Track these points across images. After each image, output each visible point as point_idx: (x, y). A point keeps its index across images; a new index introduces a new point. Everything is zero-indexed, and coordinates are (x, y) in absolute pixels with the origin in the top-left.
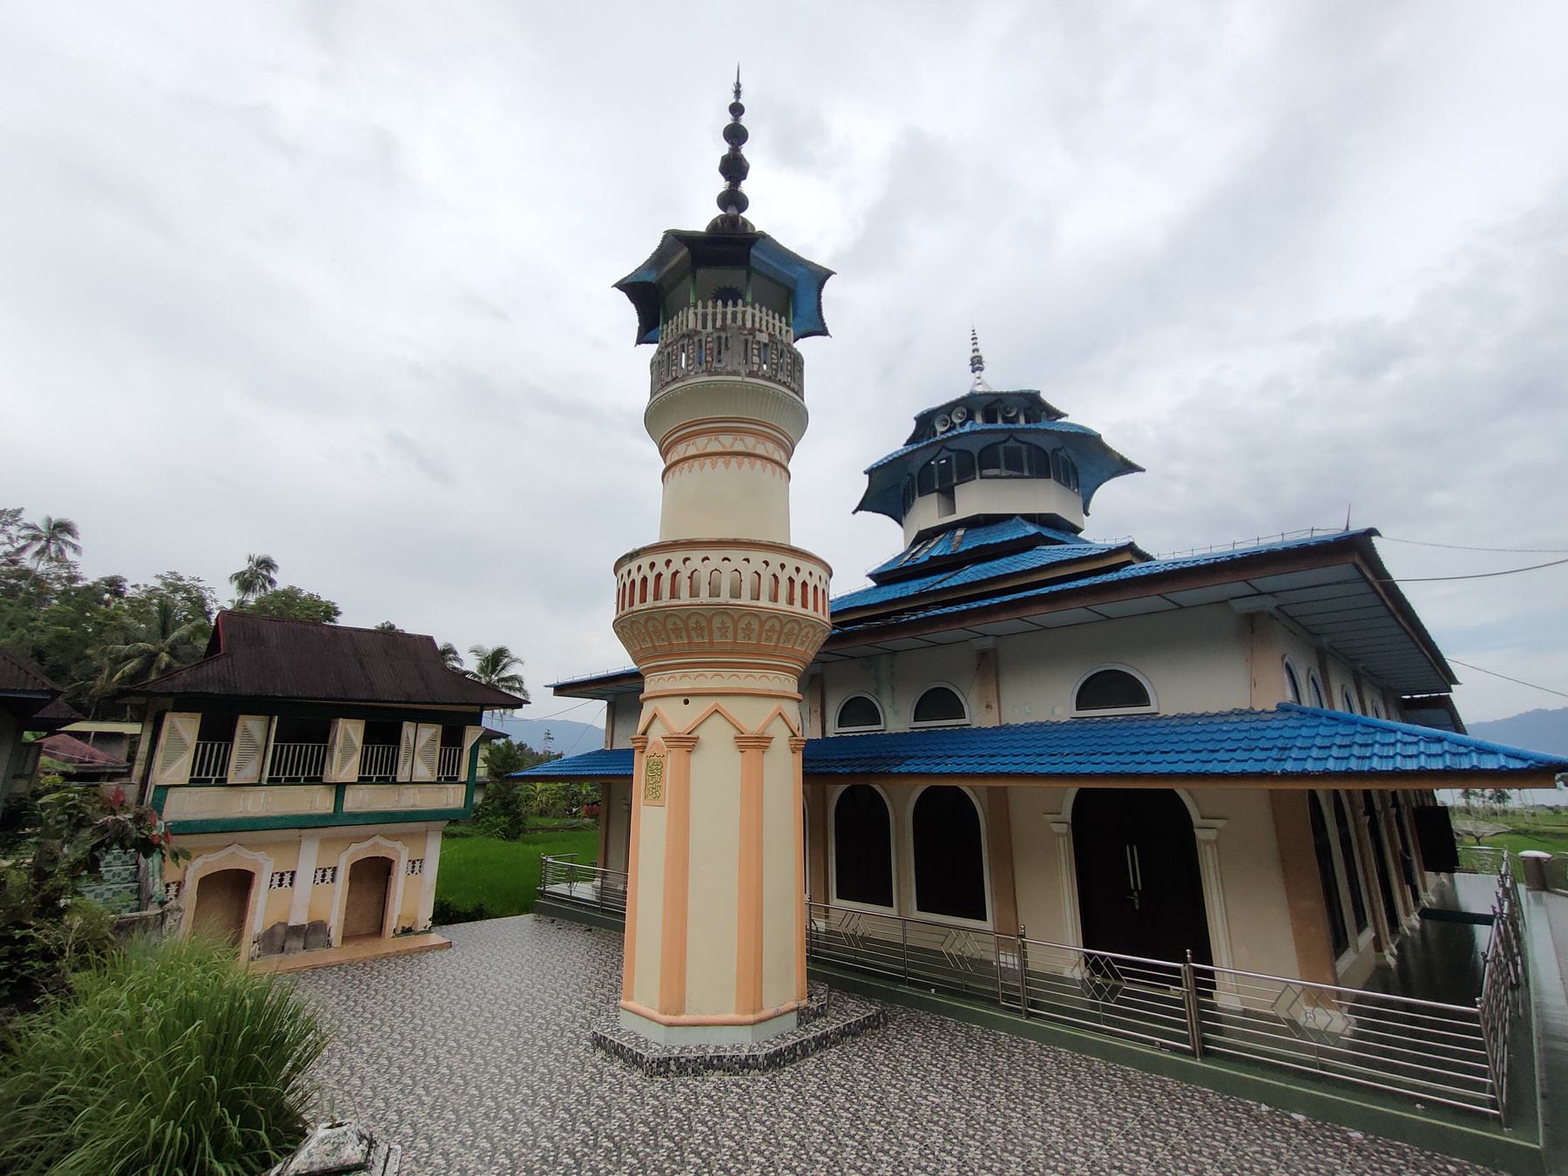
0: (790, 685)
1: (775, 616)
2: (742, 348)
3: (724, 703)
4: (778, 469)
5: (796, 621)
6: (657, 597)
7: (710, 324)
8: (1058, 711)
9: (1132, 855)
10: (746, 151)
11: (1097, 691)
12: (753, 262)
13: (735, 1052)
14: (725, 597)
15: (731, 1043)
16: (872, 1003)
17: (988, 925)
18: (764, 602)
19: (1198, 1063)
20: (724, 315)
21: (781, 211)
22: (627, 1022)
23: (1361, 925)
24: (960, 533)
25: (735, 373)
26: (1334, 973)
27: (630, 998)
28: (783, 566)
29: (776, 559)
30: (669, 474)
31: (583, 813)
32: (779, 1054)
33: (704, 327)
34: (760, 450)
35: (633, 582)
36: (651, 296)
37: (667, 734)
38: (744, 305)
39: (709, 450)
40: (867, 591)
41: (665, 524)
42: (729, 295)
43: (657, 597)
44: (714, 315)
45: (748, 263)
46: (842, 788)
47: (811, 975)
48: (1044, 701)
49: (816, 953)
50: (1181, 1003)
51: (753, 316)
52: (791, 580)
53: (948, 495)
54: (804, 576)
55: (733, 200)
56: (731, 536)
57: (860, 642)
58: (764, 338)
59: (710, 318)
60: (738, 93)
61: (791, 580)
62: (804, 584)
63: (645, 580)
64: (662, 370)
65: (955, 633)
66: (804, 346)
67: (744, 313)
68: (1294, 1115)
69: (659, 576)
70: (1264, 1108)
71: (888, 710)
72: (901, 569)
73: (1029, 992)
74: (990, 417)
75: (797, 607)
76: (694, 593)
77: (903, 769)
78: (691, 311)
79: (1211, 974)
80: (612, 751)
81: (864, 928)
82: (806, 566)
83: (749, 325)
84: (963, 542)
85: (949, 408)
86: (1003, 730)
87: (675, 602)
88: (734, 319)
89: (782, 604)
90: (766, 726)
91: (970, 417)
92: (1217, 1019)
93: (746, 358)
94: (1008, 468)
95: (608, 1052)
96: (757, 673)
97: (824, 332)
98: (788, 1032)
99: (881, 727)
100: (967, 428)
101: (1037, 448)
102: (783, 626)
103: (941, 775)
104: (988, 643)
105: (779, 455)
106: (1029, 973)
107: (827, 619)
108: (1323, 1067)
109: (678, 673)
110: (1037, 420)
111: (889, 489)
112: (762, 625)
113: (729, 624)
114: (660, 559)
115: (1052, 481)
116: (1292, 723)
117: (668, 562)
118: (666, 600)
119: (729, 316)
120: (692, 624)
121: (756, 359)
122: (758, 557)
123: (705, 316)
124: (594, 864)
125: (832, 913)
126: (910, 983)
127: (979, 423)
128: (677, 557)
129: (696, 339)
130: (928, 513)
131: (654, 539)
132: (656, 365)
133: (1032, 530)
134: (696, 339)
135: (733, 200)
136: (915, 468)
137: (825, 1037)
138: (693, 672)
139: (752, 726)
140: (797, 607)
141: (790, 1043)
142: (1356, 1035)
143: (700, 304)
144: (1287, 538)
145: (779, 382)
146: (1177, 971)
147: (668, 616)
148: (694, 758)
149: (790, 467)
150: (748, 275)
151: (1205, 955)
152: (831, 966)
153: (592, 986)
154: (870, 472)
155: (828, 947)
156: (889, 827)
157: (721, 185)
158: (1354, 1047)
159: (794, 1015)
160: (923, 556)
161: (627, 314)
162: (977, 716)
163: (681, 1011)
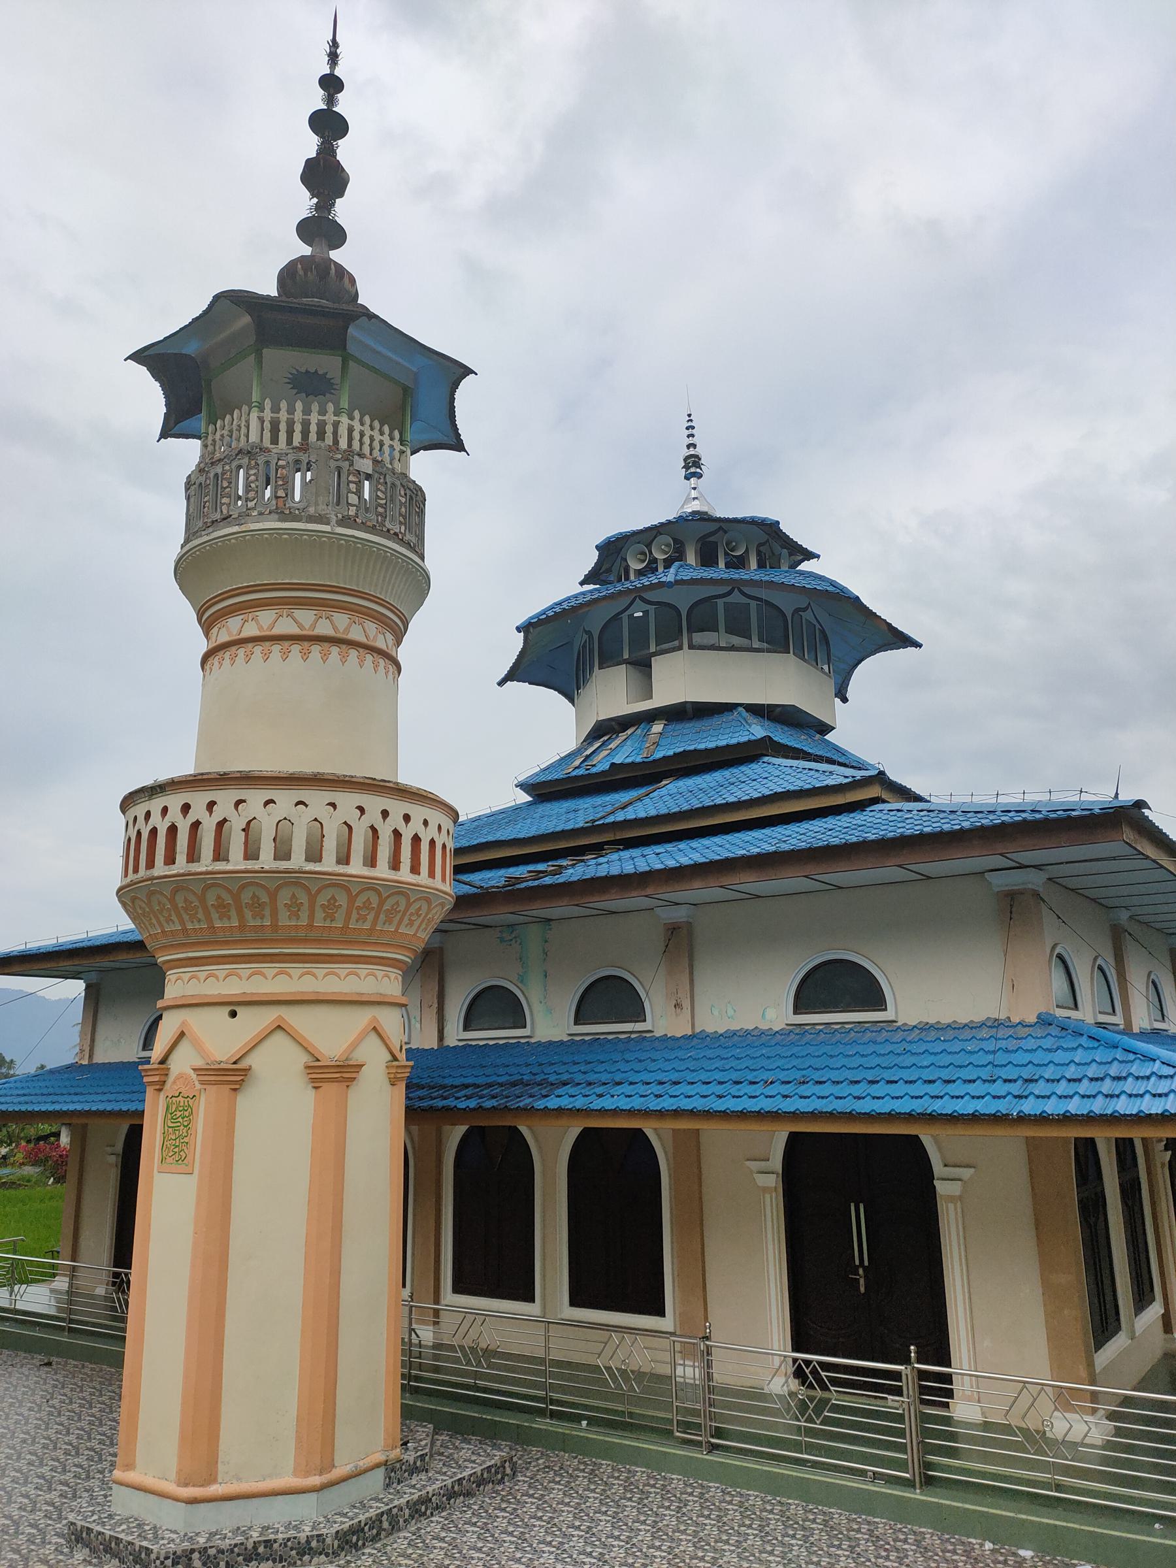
0: (389, 984)
1: (371, 886)
3: (295, 1018)
6: (193, 856)
7: (283, 436)
8: (771, 1014)
9: (858, 1216)
10: (345, 151)
11: (815, 991)
12: (351, 348)
13: (292, 1533)
14: (298, 860)
15: (286, 1519)
16: (494, 1446)
17: (666, 1323)
18: (356, 867)
19: (917, 1495)
20: (306, 425)
21: (399, 281)
22: (124, 1503)
23: (1142, 1298)
24: (657, 728)
25: (321, 519)
26: (1090, 1364)
27: (130, 1466)
28: (385, 814)
29: (375, 803)
30: (215, 661)
31: (20, 1156)
32: (357, 1530)
33: (275, 441)
34: (356, 634)
35: (154, 831)
36: (190, 374)
37: (200, 1063)
38: (337, 413)
39: (276, 631)
40: (517, 809)
41: (206, 739)
42: (311, 386)
43: (193, 856)
45: (344, 347)
46: (461, 1130)
47: (408, 1413)
48: (750, 1000)
49: (418, 1379)
50: (900, 1418)
51: (351, 430)
52: (397, 834)
53: (643, 666)
54: (416, 826)
55: (321, 229)
56: (308, 769)
57: (508, 888)
58: (366, 466)
59: (283, 427)
60: (333, 57)
61: (397, 834)
62: (416, 839)
63: (173, 830)
64: (205, 493)
65: (635, 900)
66: (425, 468)
67: (336, 425)
68: (1022, 1552)
69: (196, 825)
70: (988, 1545)
71: (537, 1007)
72: (569, 779)
73: (713, 1417)
74: (707, 559)
75: (404, 874)
76: (251, 854)
77: (552, 1103)
78: (254, 415)
79: (948, 1378)
80: (92, 1067)
81: (490, 1337)
82: (419, 812)
83: (343, 444)
84: (664, 742)
86: (697, 1039)
87: (221, 866)
88: (321, 435)
89: (382, 870)
90: (355, 1045)
91: (677, 556)
92: (953, 1437)
93: (338, 504)
94: (730, 631)
95: (93, 1551)
96: (343, 969)
97: (459, 446)
98: (370, 1496)
99: (526, 1032)
100: (670, 576)
101: (768, 603)
102: (382, 903)
103: (603, 1112)
104: (679, 915)
105: (383, 641)
106: (712, 1389)
108: (1059, 1487)
109: (221, 970)
110: (776, 566)
111: (555, 652)
112: (352, 899)
113: (303, 898)
114: (198, 800)
116: (1048, 1043)
117: (211, 805)
118: (206, 863)
119: (313, 428)
120: (246, 897)
122: (348, 801)
124: (54, 1254)
125: (445, 1317)
126: (554, 1415)
127: (691, 567)
128: (225, 798)
129: (261, 460)
130: (612, 694)
131: (187, 768)
133: (758, 730)
134: (261, 460)
135: (321, 229)
137: (425, 1500)
138: (244, 969)
139: (332, 1048)
140: (404, 874)
141: (372, 1513)
142: (1109, 1445)
143: (268, 404)
144: (1055, 797)
145: (387, 534)
146: (897, 1376)
147: (207, 887)
148: (244, 1102)
151: (940, 1352)
152: (441, 1398)
153: (59, 1454)
154: (526, 628)
155: (437, 1369)
156: (526, 1195)
157: (303, 203)
158: (1106, 1461)
159: (380, 1473)
160: (601, 763)
161: (148, 398)
162: (661, 1019)
163: (212, 1479)
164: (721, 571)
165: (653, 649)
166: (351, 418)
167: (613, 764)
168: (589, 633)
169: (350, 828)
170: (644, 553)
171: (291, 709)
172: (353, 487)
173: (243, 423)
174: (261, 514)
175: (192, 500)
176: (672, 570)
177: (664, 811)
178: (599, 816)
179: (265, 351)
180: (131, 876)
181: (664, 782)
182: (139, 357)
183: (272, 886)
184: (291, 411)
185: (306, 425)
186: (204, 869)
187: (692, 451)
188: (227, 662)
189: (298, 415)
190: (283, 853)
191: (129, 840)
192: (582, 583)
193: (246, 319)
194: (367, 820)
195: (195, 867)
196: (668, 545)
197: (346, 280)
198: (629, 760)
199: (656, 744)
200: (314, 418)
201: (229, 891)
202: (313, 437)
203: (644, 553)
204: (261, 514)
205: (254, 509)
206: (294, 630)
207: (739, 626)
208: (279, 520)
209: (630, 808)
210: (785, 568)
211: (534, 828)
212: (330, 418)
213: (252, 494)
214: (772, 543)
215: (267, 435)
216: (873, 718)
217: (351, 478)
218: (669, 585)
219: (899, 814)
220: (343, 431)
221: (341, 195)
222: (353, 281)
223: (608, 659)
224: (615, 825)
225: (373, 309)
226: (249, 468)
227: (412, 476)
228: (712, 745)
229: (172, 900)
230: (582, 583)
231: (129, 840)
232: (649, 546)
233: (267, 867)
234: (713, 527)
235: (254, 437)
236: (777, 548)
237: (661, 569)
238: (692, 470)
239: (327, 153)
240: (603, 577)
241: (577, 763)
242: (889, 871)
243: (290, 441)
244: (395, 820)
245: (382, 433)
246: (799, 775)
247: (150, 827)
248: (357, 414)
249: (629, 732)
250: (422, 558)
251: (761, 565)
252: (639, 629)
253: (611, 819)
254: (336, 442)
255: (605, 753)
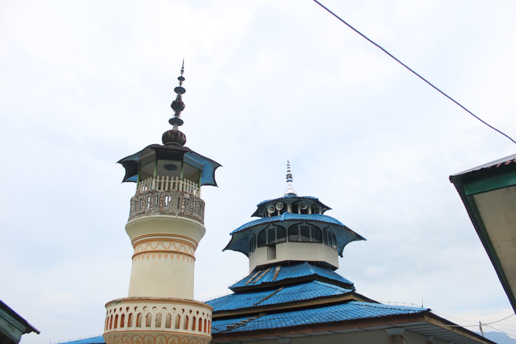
1: (186, 336)
2: (177, 202)
4: (190, 258)
5: (196, 338)
6: (129, 325)
7: (162, 187)
12: (185, 160)
14: (163, 328)
18: (181, 330)
20: (169, 183)
24: (278, 269)
25: (173, 214)
28: (191, 311)
30: (137, 257)
33: (160, 188)
34: (182, 250)
35: (117, 316)
38: (179, 180)
39: (157, 249)
40: (229, 296)
43: (129, 325)
44: (165, 183)
51: (183, 185)
52: (194, 318)
53: (273, 247)
55: (176, 121)
56: (166, 296)
58: (187, 196)
60: (182, 71)
61: (194, 318)
62: (200, 319)
63: (123, 316)
67: (179, 183)
69: (130, 314)
74: (295, 211)
78: (154, 180)
85: (275, 202)
88: (174, 188)
89: (190, 331)
93: (178, 208)
97: (215, 185)
101: (315, 226)
107: (210, 335)
111: (243, 241)
114: (132, 306)
115: (323, 245)
119: (172, 184)
121: (183, 207)
122: (179, 307)
123: (160, 183)
129: (155, 195)
130: (262, 256)
132: (136, 202)
133: (312, 271)
134: (155, 195)
135: (176, 121)
136: (257, 232)
143: (158, 177)
149: (196, 256)
150: (182, 164)
157: (171, 114)
164: (299, 216)
165: (276, 241)
166: (183, 181)
167: (263, 283)
168: (254, 234)
169: (180, 316)
170: (273, 208)
171: (160, 275)
172: (183, 203)
173: (150, 183)
174: (154, 212)
175: (133, 205)
176: (283, 216)
177: (281, 302)
178: (258, 301)
179: (158, 161)
180: (109, 330)
181: (280, 289)
182: (120, 162)
183: (154, 336)
184: (165, 179)
185: (169, 183)
186: (133, 329)
187: (289, 173)
188: (141, 259)
189: (167, 181)
190: (158, 325)
191: (108, 317)
192: (254, 215)
193: (154, 152)
194: (185, 314)
195: (130, 329)
196: (281, 205)
197: (183, 137)
198: (268, 281)
199: (277, 275)
200: (172, 181)
201: (141, 337)
202: (171, 187)
203: (273, 208)
204: (154, 212)
205: (152, 210)
206: (163, 249)
207: (305, 233)
208: (161, 214)
209: (269, 300)
210: (320, 214)
211: (235, 306)
212: (177, 181)
213: (152, 206)
214: (317, 206)
215: (157, 187)
216: (350, 264)
217: (183, 200)
218: (282, 221)
219: (359, 306)
220: (181, 185)
221: (182, 110)
222: (185, 137)
223: (261, 244)
224: (264, 306)
225: (192, 149)
226: (151, 197)
227: (201, 198)
228: (296, 276)
229: (122, 339)
230: (254, 215)
231: (108, 317)
232: (275, 205)
233: (153, 330)
234: (297, 200)
235: (153, 188)
236: (318, 205)
237: (279, 214)
238: (289, 179)
239: (179, 98)
240: (259, 214)
241: (250, 281)
242: (355, 329)
243: (164, 188)
244: (194, 314)
245: (192, 185)
246: (327, 289)
247: (116, 314)
248: (185, 180)
249: (268, 270)
250: (203, 224)
251: (313, 212)
252: (272, 232)
253: (262, 304)
254: (178, 189)
255: (260, 278)
